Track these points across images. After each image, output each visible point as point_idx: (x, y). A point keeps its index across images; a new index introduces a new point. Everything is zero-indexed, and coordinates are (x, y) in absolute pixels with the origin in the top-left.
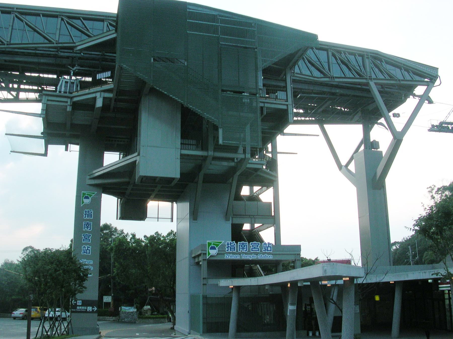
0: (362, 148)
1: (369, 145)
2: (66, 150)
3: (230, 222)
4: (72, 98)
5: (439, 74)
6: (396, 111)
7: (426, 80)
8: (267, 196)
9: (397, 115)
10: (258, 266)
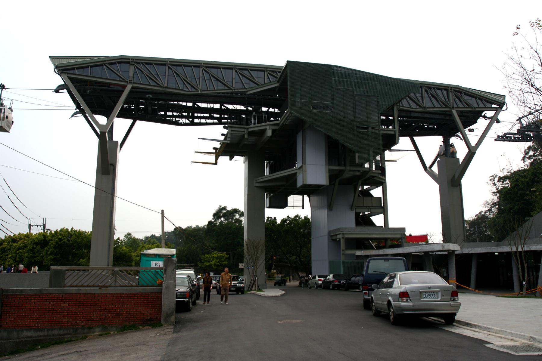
1: (447, 152)
2: (231, 159)
3: (354, 211)
4: (248, 128)
6: (471, 127)
7: (493, 106)
8: (377, 192)
9: (472, 130)
10: (52, 267)
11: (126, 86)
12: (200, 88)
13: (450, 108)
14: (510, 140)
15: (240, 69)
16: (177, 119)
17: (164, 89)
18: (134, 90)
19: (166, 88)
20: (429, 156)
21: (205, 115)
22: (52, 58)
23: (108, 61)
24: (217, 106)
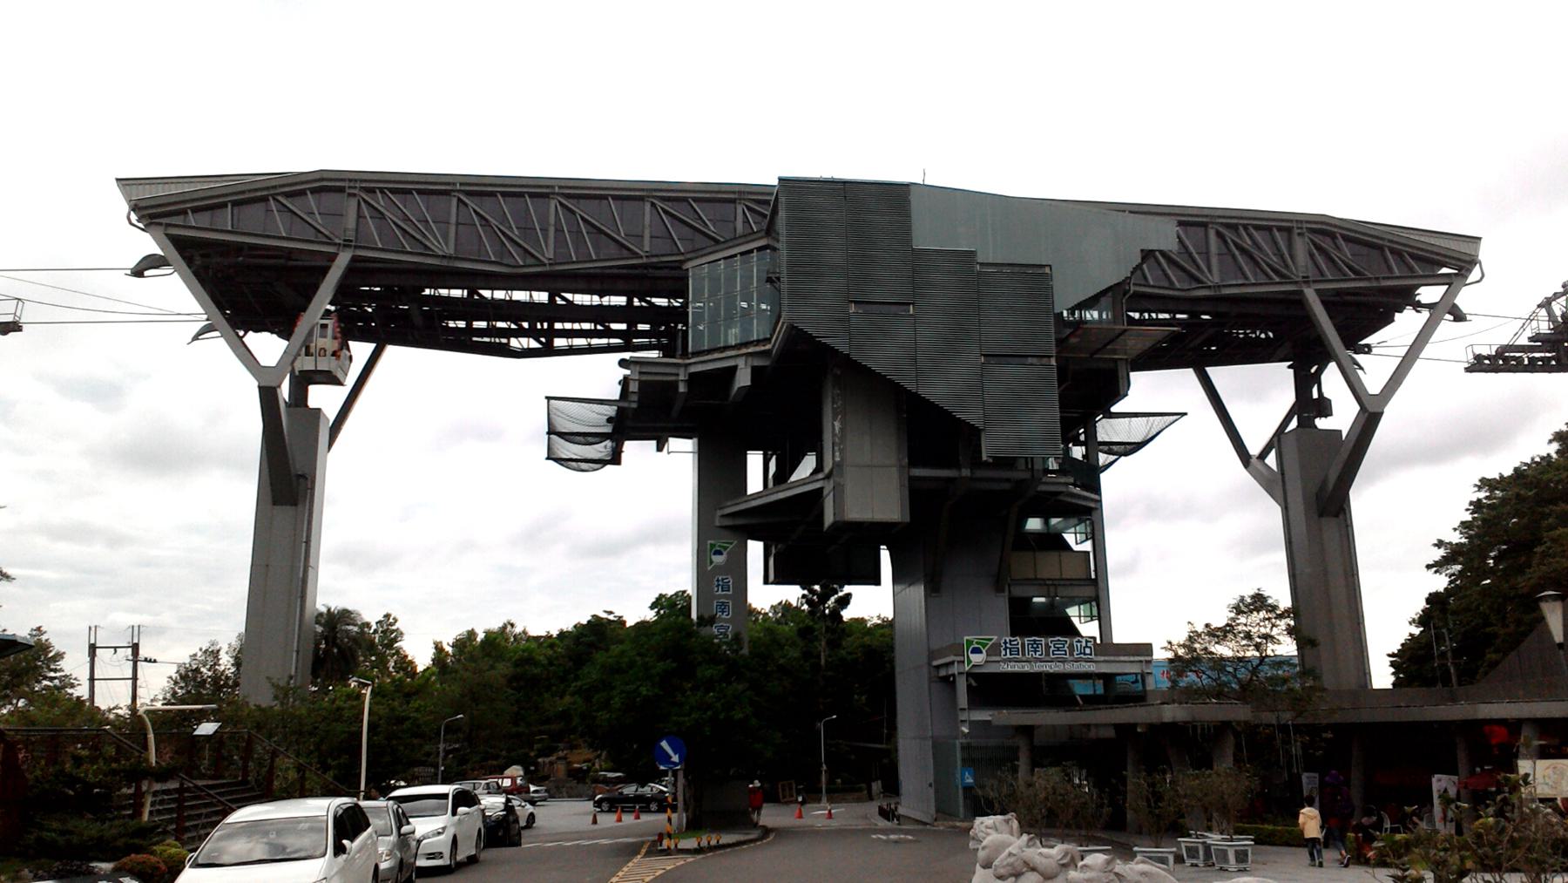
0: (1294, 424)
2: (660, 449)
4: (687, 366)
5: (1480, 257)
7: (1445, 270)
13: (1296, 283)
14: (1519, 367)
15: (663, 199)
17: (445, 263)
19: (450, 257)
20: (1258, 427)
21: (586, 326)
22: (118, 180)
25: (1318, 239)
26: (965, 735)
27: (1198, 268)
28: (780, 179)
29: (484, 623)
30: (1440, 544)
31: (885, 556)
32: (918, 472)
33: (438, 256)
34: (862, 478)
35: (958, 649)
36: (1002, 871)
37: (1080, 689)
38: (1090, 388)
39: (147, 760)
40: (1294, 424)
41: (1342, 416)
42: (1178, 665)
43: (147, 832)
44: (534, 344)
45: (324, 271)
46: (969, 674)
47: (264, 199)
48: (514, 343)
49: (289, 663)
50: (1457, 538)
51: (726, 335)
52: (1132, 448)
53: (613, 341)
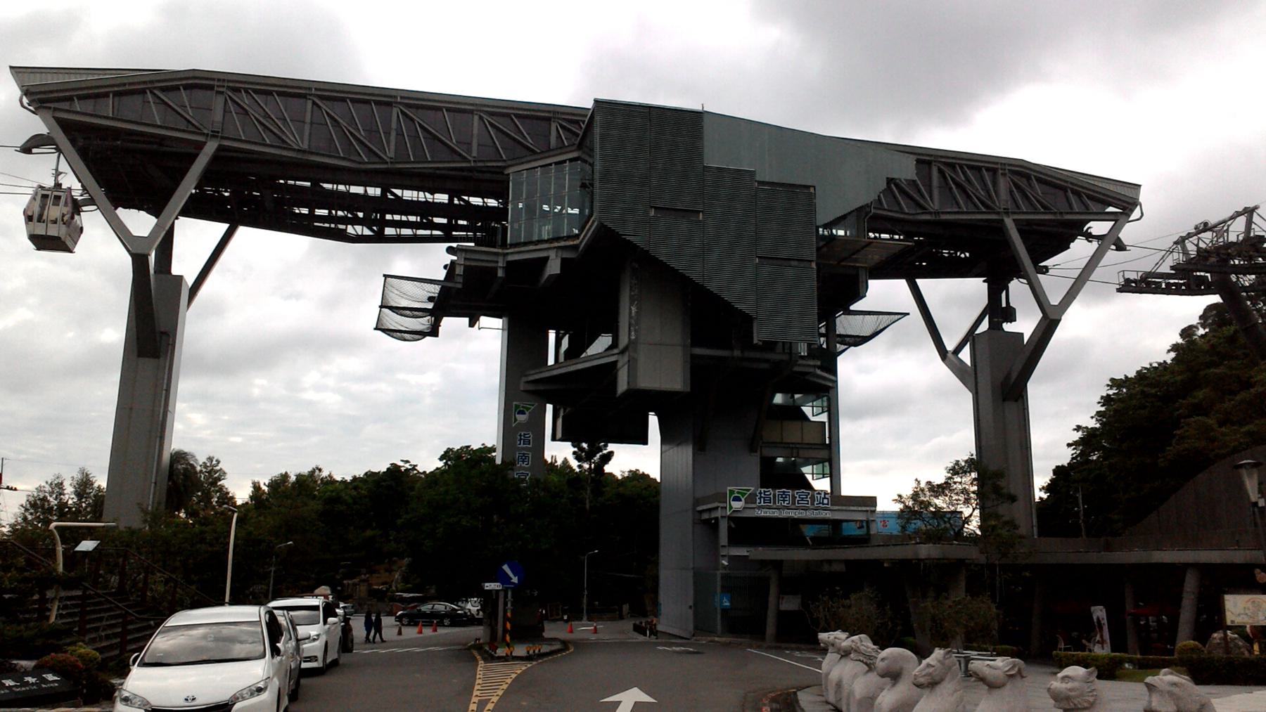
0: (984, 326)
2: (472, 325)
5: (1141, 199)
7: (1111, 209)
11: (205, 143)
12: (392, 155)
13: (998, 213)
14: (1157, 290)
15: (492, 114)
16: (341, 227)
18: (223, 154)
19: (304, 152)
21: (412, 218)
23: (159, 81)
24: (442, 198)
25: (1016, 178)
26: (725, 567)
27: (922, 196)
28: (596, 101)
29: (296, 467)
30: (1078, 428)
31: (653, 420)
32: (698, 351)
33: (294, 150)
34: (651, 354)
35: (722, 497)
36: (922, 680)
37: (809, 531)
38: (841, 290)
39: (55, 570)
40: (984, 326)
41: (1025, 325)
42: (907, 515)
43: (58, 633)
44: (367, 232)
45: (192, 158)
46: (730, 518)
47: (143, 92)
48: (350, 229)
49: (152, 496)
50: (1093, 424)
51: (540, 231)
52: (859, 340)
53: (436, 233)
